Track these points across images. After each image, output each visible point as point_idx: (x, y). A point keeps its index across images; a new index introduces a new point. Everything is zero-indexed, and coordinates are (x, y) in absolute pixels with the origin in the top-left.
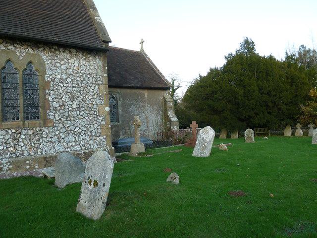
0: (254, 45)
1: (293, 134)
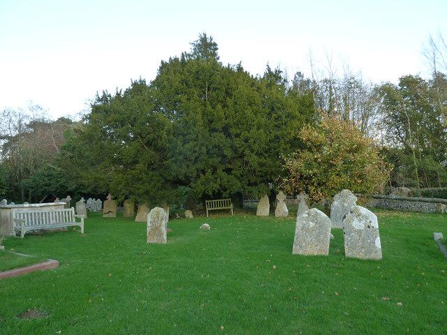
0: (217, 49)
1: (272, 209)
